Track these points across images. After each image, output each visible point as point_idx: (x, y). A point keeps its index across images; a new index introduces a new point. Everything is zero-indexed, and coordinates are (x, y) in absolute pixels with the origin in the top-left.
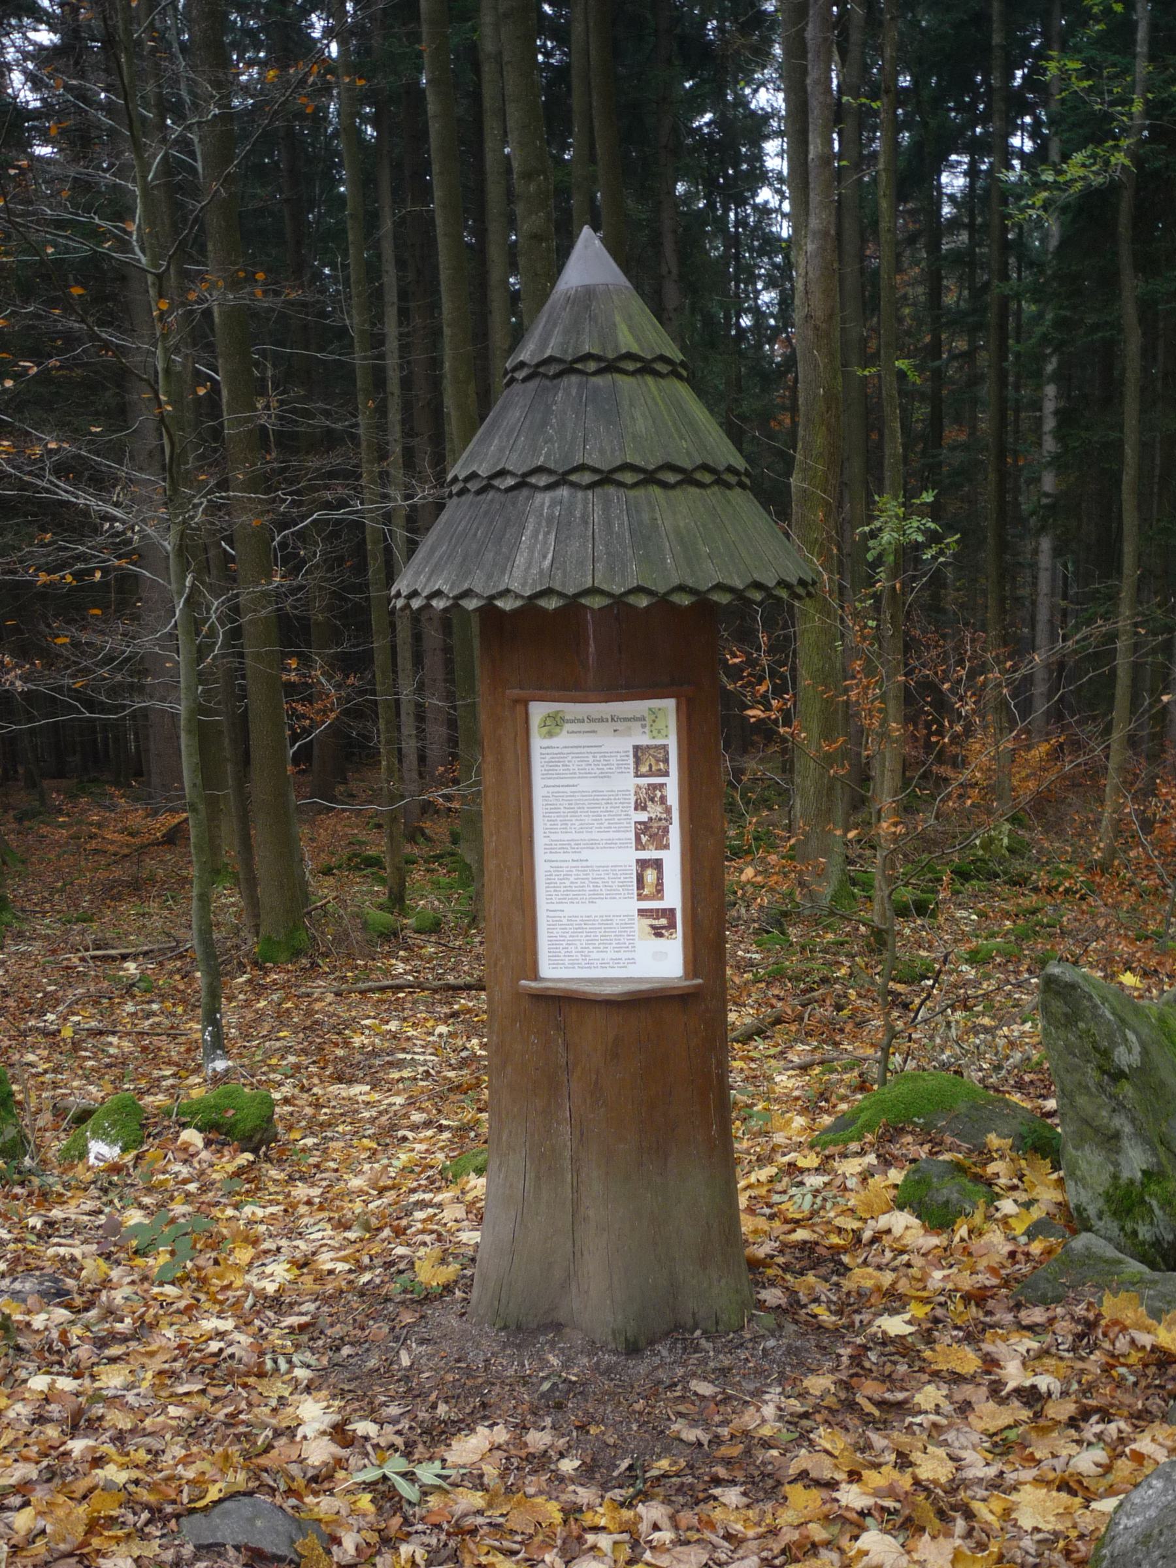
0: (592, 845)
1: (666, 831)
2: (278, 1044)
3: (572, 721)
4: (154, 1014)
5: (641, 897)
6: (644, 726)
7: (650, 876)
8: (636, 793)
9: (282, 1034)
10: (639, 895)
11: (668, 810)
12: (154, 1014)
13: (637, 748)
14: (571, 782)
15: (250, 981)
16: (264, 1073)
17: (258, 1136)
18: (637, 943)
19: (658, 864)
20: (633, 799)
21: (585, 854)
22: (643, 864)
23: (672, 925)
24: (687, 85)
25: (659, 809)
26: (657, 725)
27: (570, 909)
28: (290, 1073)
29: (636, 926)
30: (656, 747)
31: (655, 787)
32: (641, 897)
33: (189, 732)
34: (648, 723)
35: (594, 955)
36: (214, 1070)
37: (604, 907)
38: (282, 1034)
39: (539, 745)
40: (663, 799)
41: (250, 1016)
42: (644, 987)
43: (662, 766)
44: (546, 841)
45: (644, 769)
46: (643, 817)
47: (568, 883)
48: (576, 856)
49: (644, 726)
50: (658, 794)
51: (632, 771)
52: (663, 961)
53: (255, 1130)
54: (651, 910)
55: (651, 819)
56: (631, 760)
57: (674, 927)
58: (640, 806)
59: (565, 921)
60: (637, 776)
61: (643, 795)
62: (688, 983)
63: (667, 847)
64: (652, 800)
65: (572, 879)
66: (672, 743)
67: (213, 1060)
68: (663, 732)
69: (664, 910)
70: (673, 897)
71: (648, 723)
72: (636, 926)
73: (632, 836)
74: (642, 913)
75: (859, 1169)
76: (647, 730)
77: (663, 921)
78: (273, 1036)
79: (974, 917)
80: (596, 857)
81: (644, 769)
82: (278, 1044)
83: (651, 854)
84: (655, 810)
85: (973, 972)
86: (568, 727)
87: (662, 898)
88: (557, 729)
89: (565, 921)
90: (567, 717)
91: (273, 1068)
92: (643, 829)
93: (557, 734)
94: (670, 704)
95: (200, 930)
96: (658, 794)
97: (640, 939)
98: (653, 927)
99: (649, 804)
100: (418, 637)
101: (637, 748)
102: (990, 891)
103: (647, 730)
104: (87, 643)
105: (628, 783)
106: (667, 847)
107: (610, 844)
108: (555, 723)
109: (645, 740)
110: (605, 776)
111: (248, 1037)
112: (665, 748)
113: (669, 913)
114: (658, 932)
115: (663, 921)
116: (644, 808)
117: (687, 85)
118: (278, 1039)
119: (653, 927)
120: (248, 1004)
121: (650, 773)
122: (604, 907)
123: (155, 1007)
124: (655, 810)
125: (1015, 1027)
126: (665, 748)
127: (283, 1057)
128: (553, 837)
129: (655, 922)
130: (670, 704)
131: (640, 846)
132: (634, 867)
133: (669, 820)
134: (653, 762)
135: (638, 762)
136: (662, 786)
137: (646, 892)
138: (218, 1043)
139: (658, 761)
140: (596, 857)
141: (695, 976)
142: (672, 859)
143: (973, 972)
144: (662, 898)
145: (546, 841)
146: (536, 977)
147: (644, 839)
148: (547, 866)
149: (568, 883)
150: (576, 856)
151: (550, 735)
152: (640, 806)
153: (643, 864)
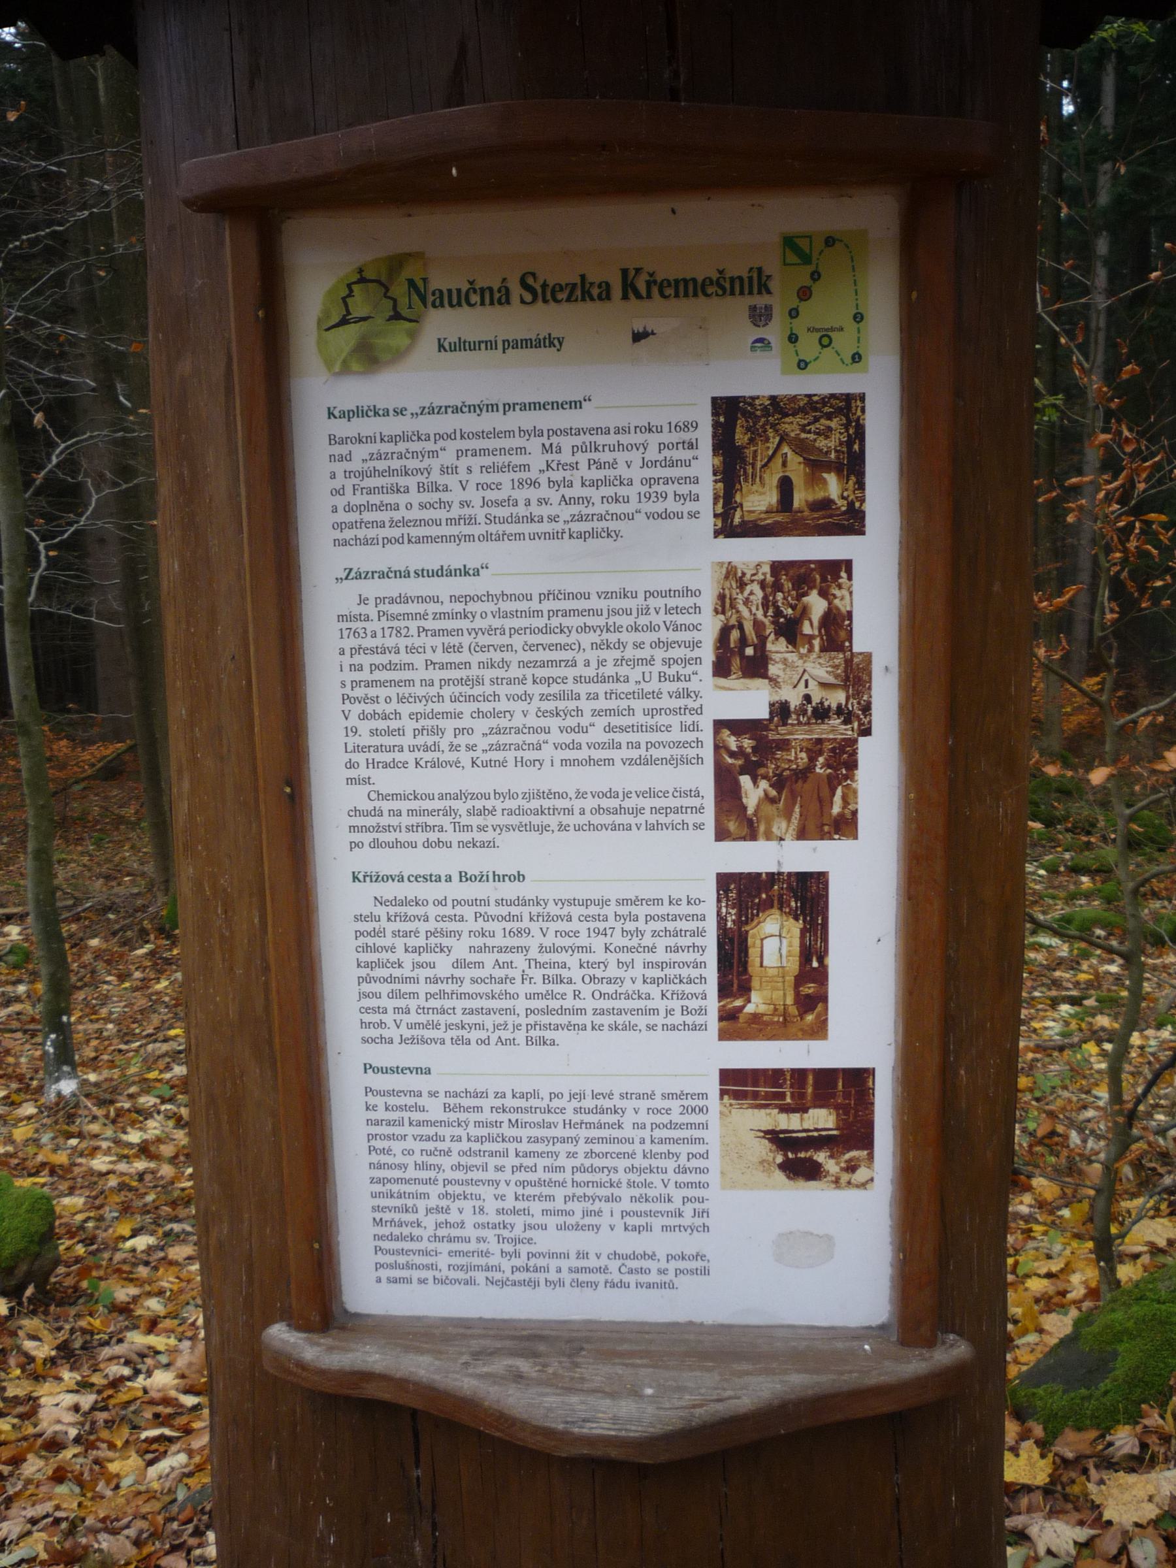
0: (539, 814)
1: (844, 760)
2: (165, 1047)
3: (457, 299)
4: (18, 999)
5: (733, 1025)
6: (760, 316)
7: (775, 941)
8: (723, 603)
9: (172, 1032)
10: (728, 1016)
11: (856, 676)
12: (18, 999)
13: (728, 410)
14: (454, 555)
15: (152, 953)
16: (131, 1096)
17: (24, 1268)
18: (717, 1197)
19: (807, 896)
20: (709, 626)
21: (513, 851)
22: (745, 894)
23: (856, 1134)
25: (820, 668)
27: (454, 1067)
28: (168, 1093)
29: (713, 1136)
30: (813, 406)
31: (801, 576)
32: (733, 1025)
33: (15, 622)
35: (545, 1241)
36: (59, 1094)
37: (588, 1061)
38: (172, 1032)
39: (326, 399)
40: (836, 629)
41: (142, 1002)
42: (754, 1391)
43: (833, 486)
44: (358, 797)
45: (758, 500)
46: (751, 701)
47: (443, 965)
48: (474, 860)
49: (760, 316)
50: (817, 605)
51: (706, 506)
52: (815, 1265)
53: (16, 1258)
54: (775, 1076)
55: (781, 710)
56: (705, 463)
57: (867, 1142)
58: (738, 657)
59: (434, 1109)
60: (728, 528)
61: (752, 609)
62: (915, 1365)
63: (846, 826)
64: (790, 631)
65: (460, 949)
66: (879, 391)
67: (58, 1080)
68: (844, 343)
69: (826, 1078)
70: (863, 1025)
72: (713, 1136)
73: (703, 778)
74: (738, 1084)
75: (1150, 1512)
76: (774, 332)
77: (822, 1119)
78: (160, 1036)
79: (1042, 872)
80: (557, 865)
81: (758, 500)
82: (165, 1047)
83: (780, 854)
84: (801, 674)
85: (1066, 947)
86: (441, 323)
87: (819, 1031)
88: (397, 336)
89: (434, 1109)
91: (147, 1087)
92: (748, 751)
93: (398, 356)
95: (37, 901)
96: (817, 605)
97: (729, 1183)
98: (778, 1139)
99: (777, 647)
101: (728, 410)
102: (1052, 840)
105: (690, 560)
106: (846, 826)
107: (615, 813)
108: (393, 300)
109: (763, 377)
110: (596, 531)
111: (126, 1036)
112: (847, 408)
113: (848, 1088)
114: (797, 1160)
115: (822, 1119)
116: (757, 668)
118: (166, 1040)
119: (778, 1139)
120: (145, 983)
121: (788, 519)
122: (588, 1061)
123: (22, 989)
124: (801, 674)
125: (1150, 1032)
126: (847, 408)
127: (168, 1068)
128: (386, 780)
129: (791, 1122)
131: (734, 820)
132: (710, 908)
133: (858, 717)
134: (796, 469)
135: (732, 469)
136: (835, 571)
137: (756, 1003)
138: (65, 1057)
139: (817, 466)
140: (557, 865)
142: (865, 876)
143: (1066, 947)
144: (819, 1031)
145: (358, 797)
146: (323, 1310)
147: (753, 792)
148: (362, 898)
149: (443, 965)
150: (474, 860)
151: (368, 358)
152: (738, 657)
153: (745, 894)
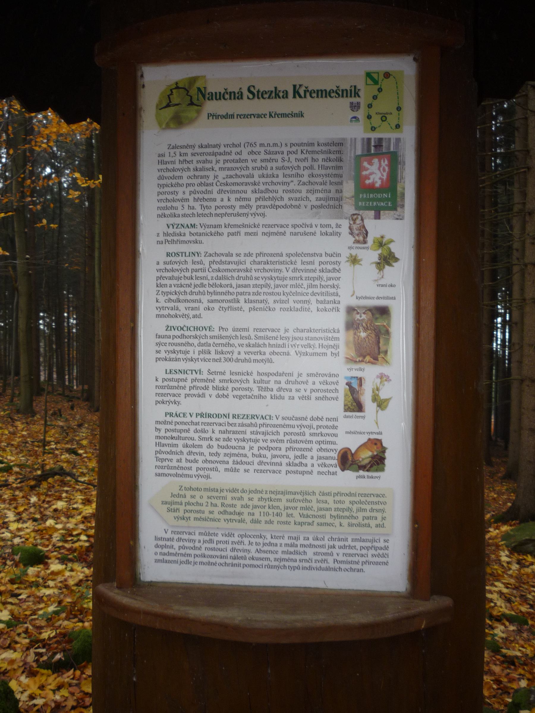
6: (355, 107)
24: (269, 671)
26: (380, 106)
34: (363, 100)
66: (407, 138)
68: (393, 120)
71: (363, 100)
76: (361, 114)
86: (211, 106)
88: (191, 112)
90: (211, 89)
93: (191, 121)
94: (404, 68)
100: (181, 380)
103: (361, 114)
104: (501, 704)
108: (185, 103)
117: (269, 671)
130: (404, 68)
141: (436, 590)
151: (178, 122)
